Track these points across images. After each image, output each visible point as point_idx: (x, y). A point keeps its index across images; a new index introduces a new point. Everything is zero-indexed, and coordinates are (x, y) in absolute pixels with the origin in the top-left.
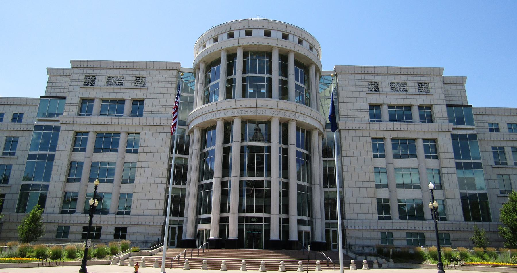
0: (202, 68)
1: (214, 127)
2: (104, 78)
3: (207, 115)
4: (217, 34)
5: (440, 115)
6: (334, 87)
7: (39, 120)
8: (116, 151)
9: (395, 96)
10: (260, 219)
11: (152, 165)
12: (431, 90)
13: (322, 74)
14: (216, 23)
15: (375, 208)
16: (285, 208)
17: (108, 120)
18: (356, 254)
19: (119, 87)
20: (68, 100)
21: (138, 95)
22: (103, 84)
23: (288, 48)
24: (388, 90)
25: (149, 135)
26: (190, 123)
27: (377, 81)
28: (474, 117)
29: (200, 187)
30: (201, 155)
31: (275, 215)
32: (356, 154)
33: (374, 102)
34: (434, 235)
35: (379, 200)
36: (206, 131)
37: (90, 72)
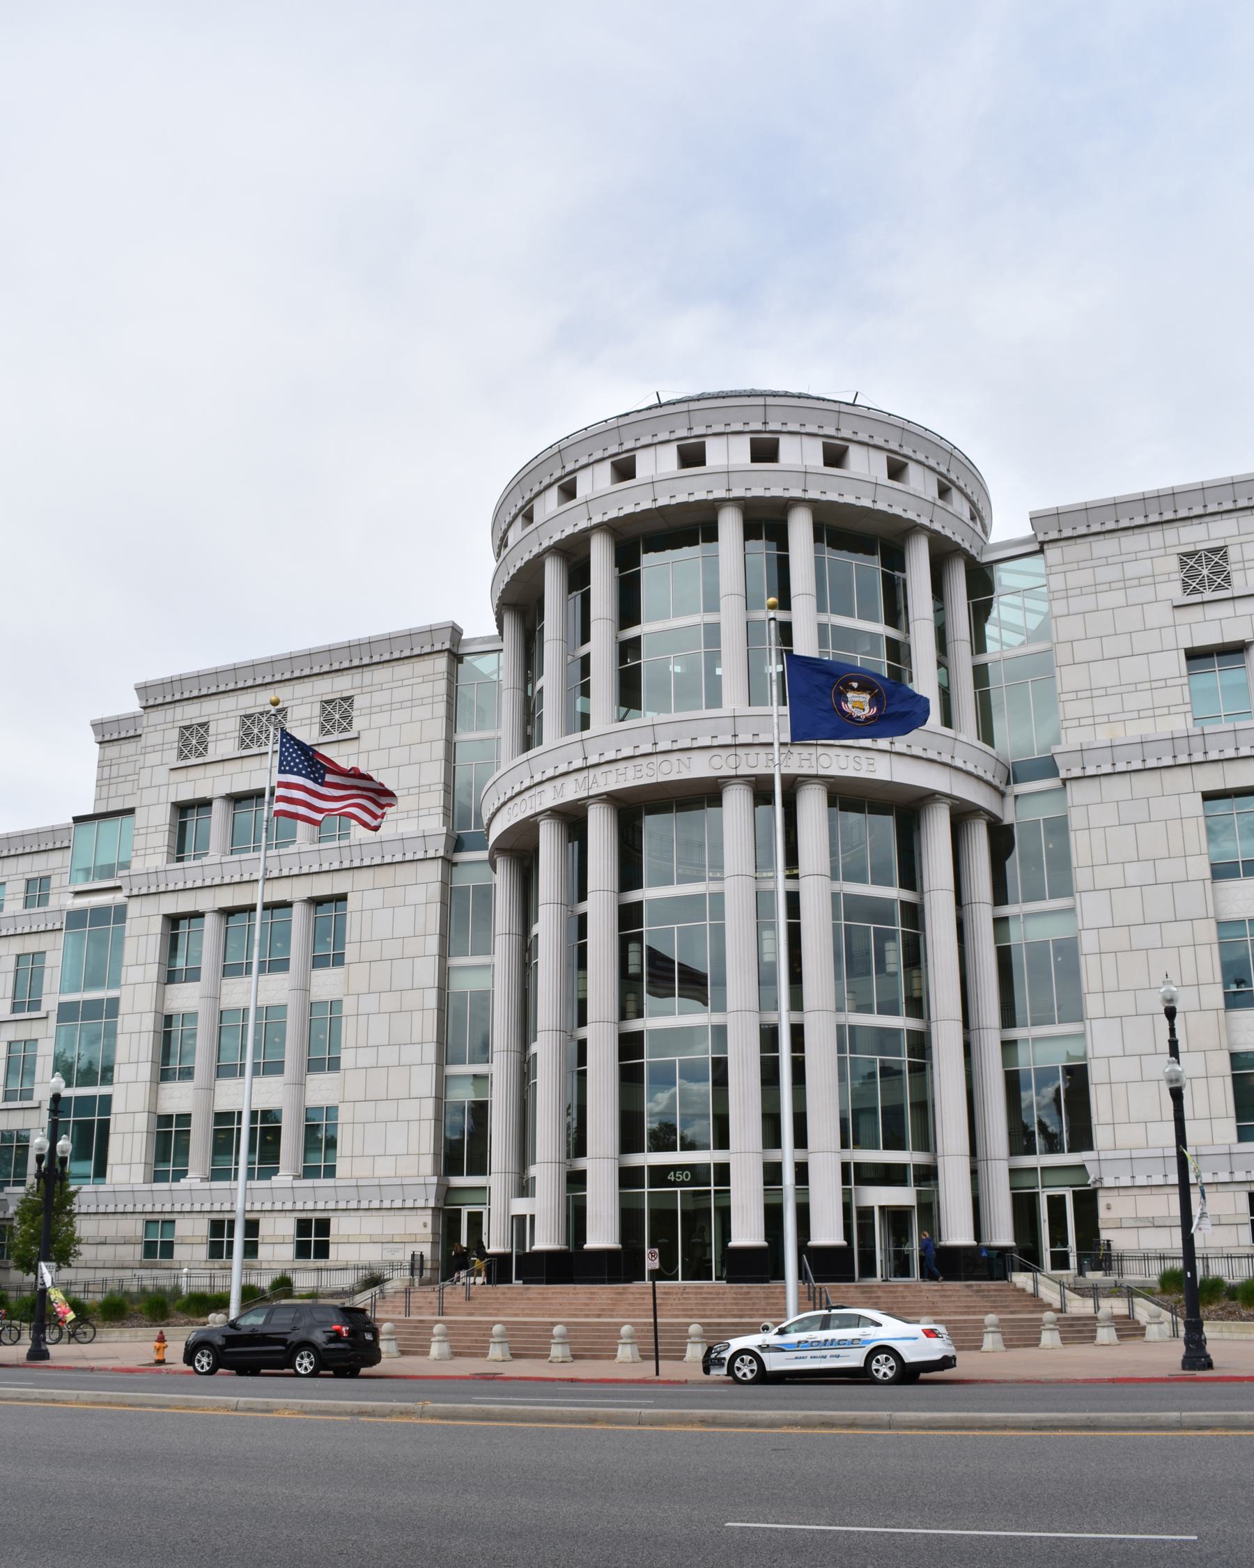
2: (231, 726)
7: (78, 894)
11: (389, 1002)
20: (140, 817)
25: (373, 899)
27: (1220, 544)
31: (745, 1156)
32: (1135, 873)
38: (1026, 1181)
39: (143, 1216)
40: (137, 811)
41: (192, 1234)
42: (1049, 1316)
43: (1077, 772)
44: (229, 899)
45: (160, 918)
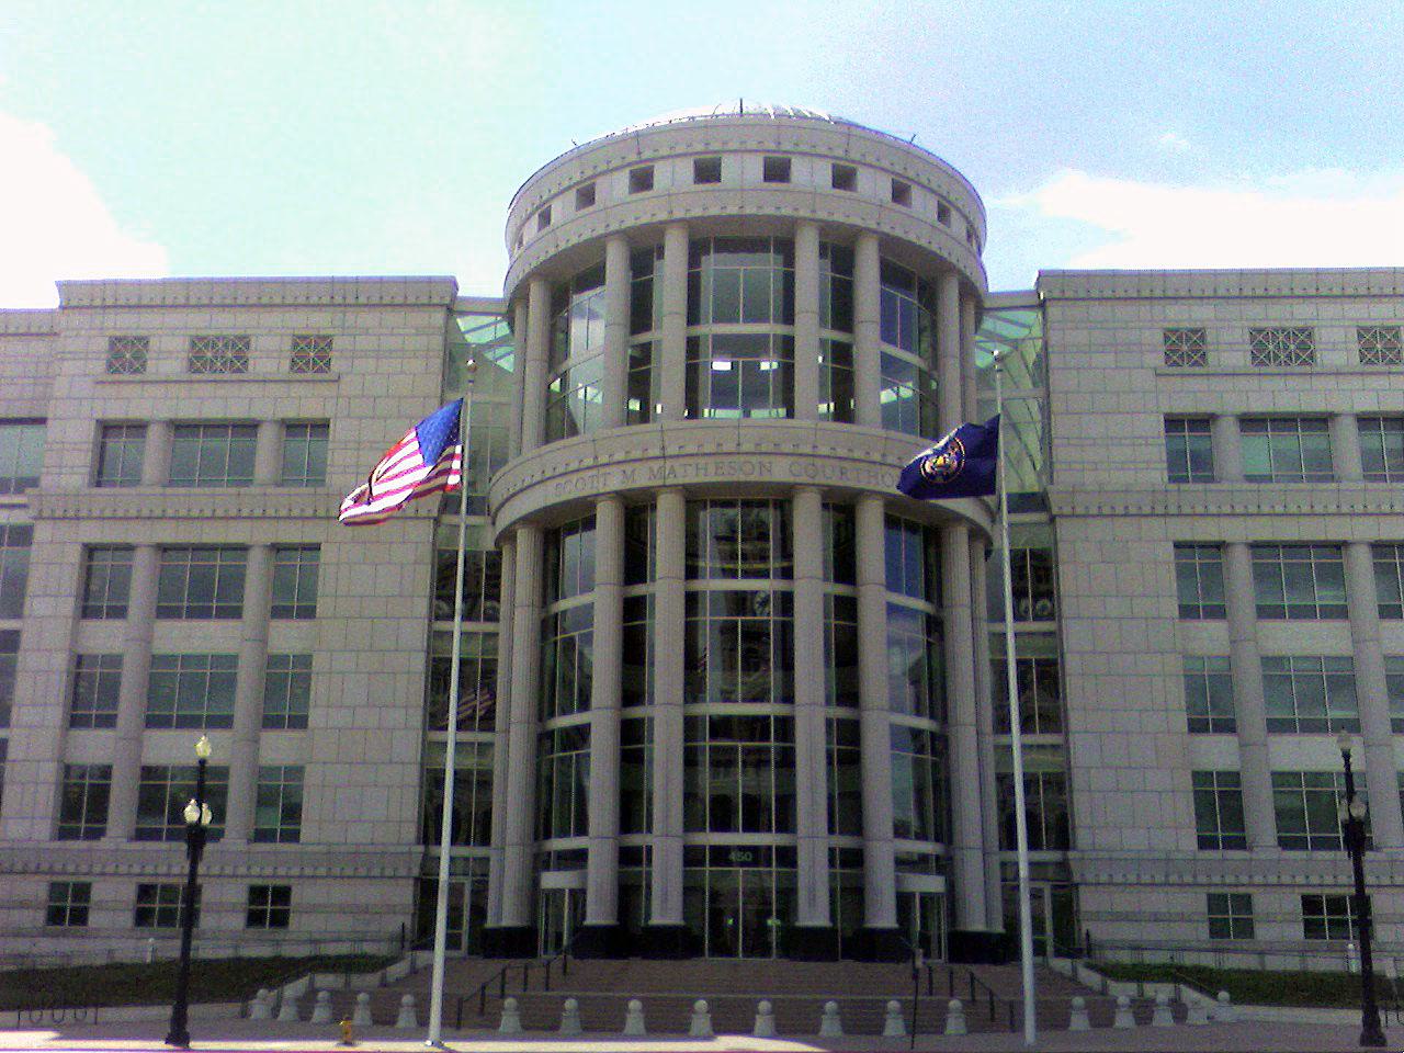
0: (537, 294)
1: (590, 524)
2: (180, 345)
3: (562, 480)
4: (589, 172)
6: (1038, 348)
8: (235, 613)
9: (1267, 383)
10: (757, 855)
13: (987, 304)
14: (593, 131)
15: (1185, 809)
16: (848, 809)
17: (199, 498)
18: (363, 985)
19: (235, 376)
20: (53, 430)
21: (306, 403)
22: (174, 367)
23: (855, 220)
24: (1240, 359)
26: (498, 509)
27: (1199, 325)
29: (544, 739)
30: (544, 622)
31: (813, 840)
33: (1185, 405)
35: (1201, 778)
36: (556, 529)
37: (127, 324)
39: (1206, 890)
40: (50, 422)
41: (112, 900)
44: (1264, 531)
45: (79, 548)
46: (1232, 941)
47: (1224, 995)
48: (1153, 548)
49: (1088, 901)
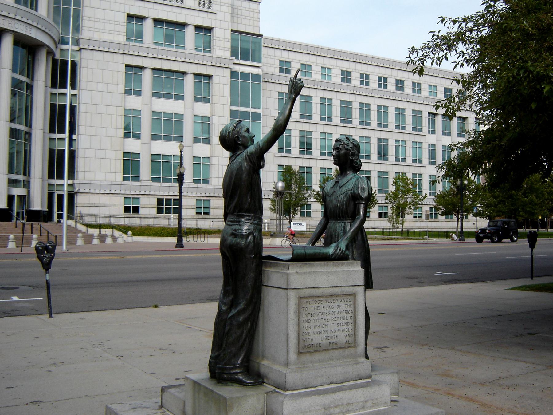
5: (221, 44)
12: (214, 6)
28: (263, 49)
32: (100, 87)
34: (184, 212)
38: (51, 188)
42: (80, 235)
43: (86, 47)
44: (158, 64)
46: (132, 215)
47: (130, 233)
48: (118, 65)
49: (79, 200)
